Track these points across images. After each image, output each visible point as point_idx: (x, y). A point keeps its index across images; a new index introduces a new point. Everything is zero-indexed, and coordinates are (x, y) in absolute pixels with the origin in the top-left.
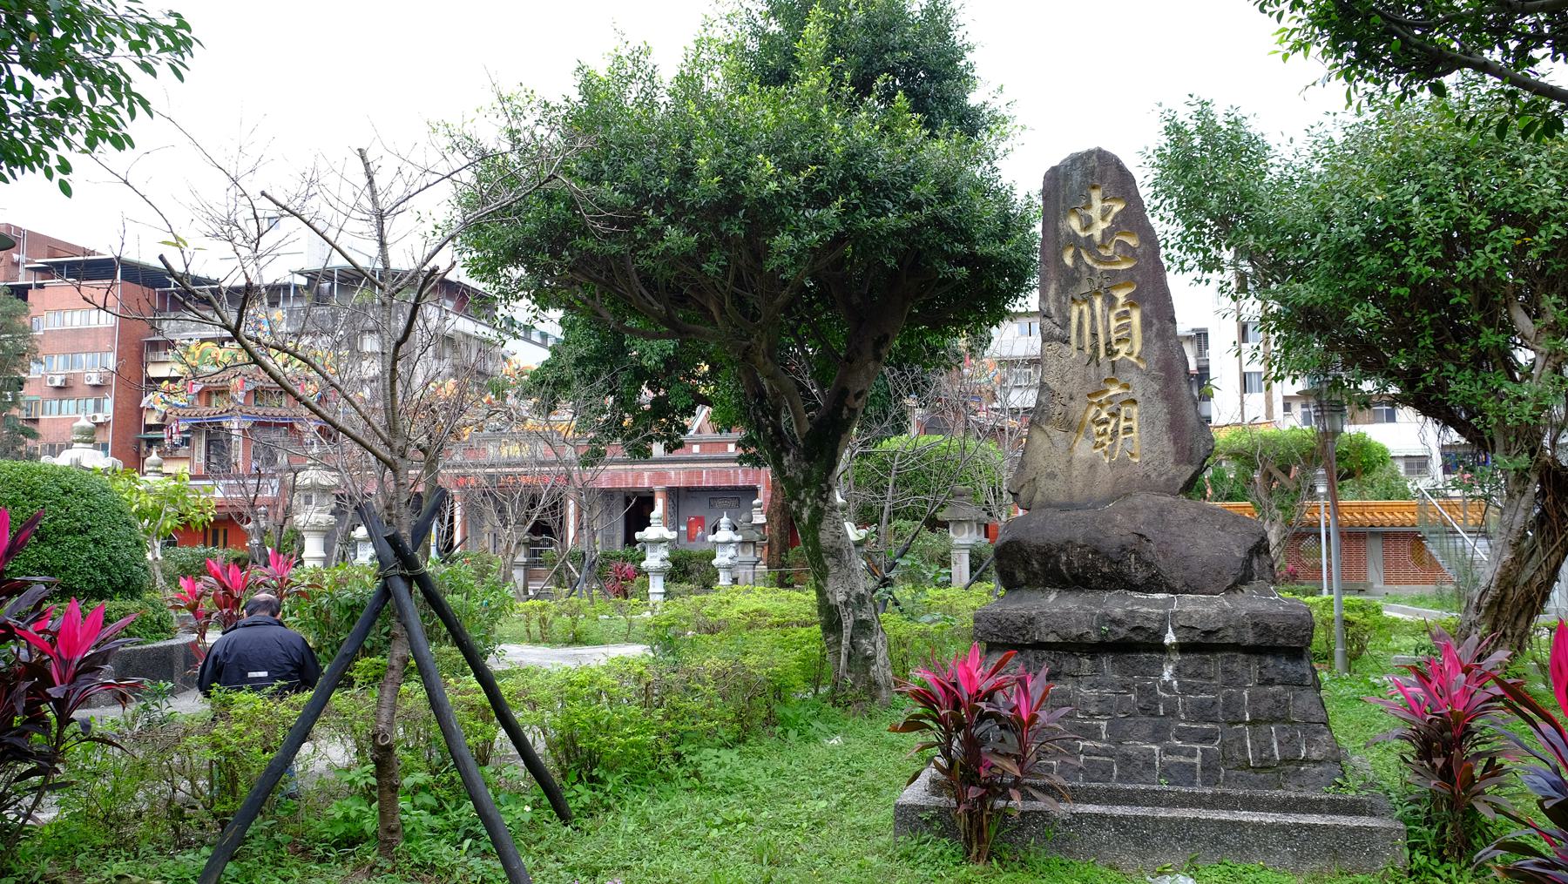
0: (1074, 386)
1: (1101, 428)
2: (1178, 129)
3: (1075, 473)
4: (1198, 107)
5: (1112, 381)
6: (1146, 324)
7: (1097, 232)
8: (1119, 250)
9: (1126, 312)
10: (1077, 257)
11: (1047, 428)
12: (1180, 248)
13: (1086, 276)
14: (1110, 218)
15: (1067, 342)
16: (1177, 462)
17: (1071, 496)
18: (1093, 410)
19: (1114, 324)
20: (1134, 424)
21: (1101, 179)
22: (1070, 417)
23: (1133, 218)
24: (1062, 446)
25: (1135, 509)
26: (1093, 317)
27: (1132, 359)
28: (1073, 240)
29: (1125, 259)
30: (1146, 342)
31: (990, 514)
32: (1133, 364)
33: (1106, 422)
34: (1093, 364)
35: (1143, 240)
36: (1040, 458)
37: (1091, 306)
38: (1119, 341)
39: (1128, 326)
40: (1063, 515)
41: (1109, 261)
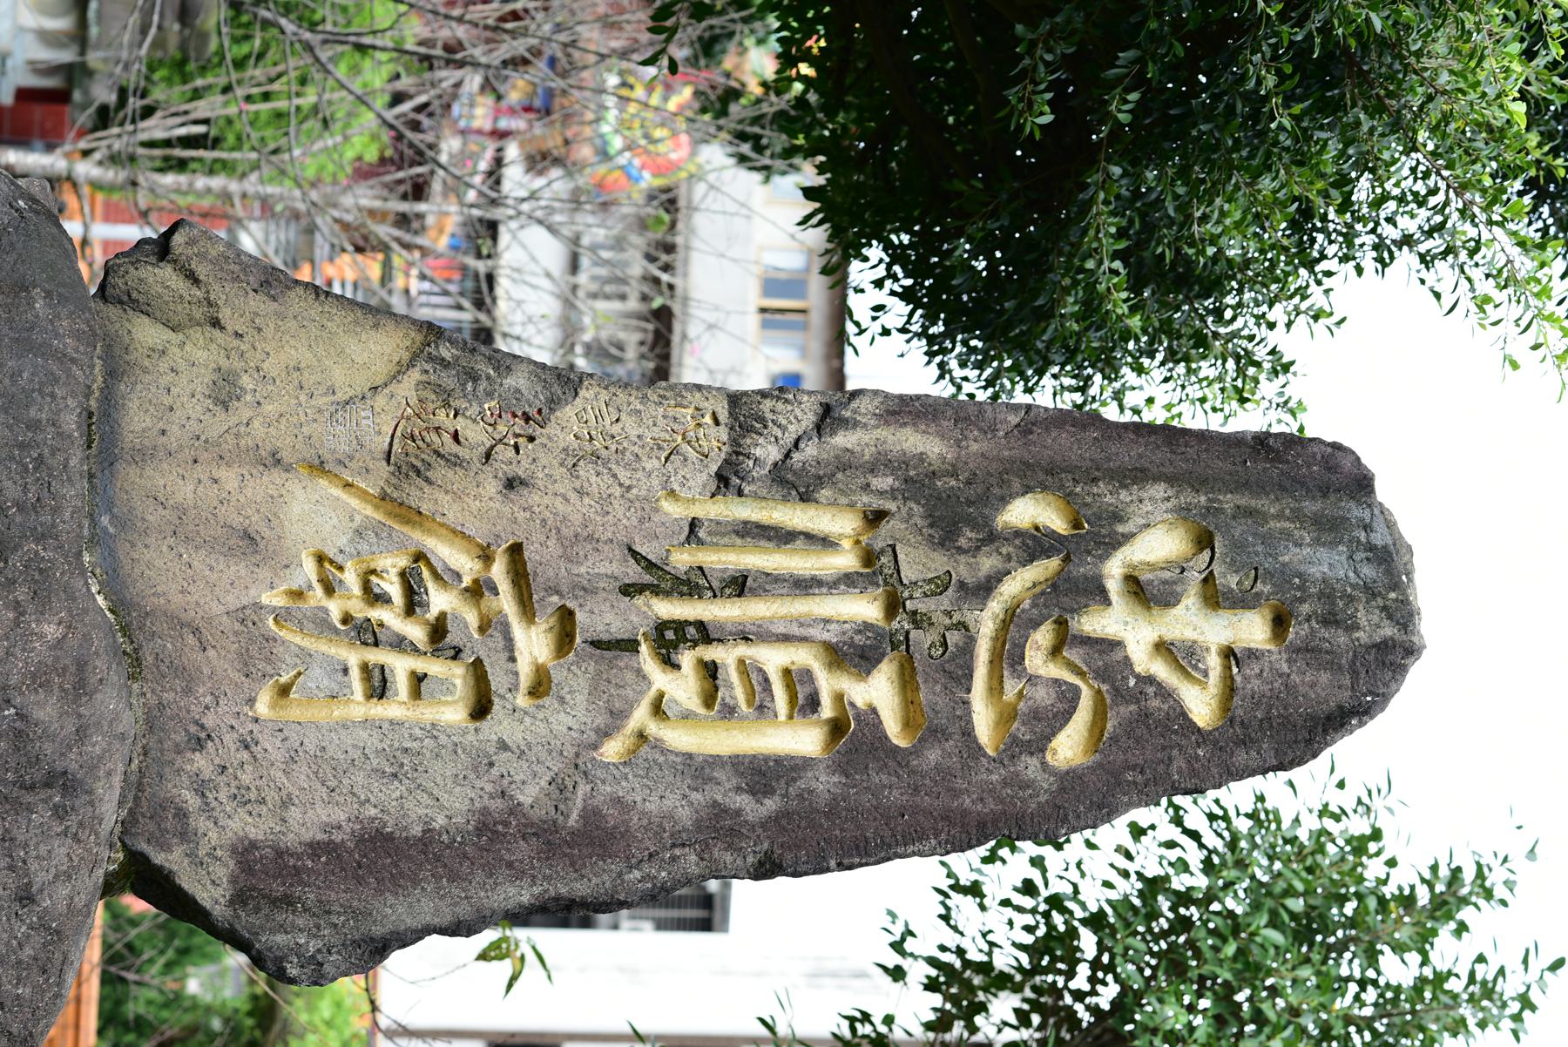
0: (559, 499)
1: (394, 590)
2: (1444, 907)
3: (229, 477)
4: (1510, 988)
5: (565, 636)
6: (763, 774)
7: (1114, 620)
8: (1043, 696)
9: (813, 703)
10: (1035, 544)
11: (407, 387)
12: (1028, 888)
13: (962, 570)
14: (1161, 670)
15: (726, 481)
16: (245, 852)
17: (143, 456)
18: (466, 565)
19: (773, 659)
20: (395, 708)
21: (1308, 651)
22: (440, 472)
23: (1150, 754)
24: (336, 439)
25: (81, 689)
26: (804, 586)
27: (640, 716)
28: (1100, 532)
29: (1007, 716)
30: (699, 769)
31: (104, 118)
32: (618, 716)
33: (413, 603)
34: (634, 573)
35: (1070, 779)
36: (296, 352)
37: (847, 581)
38: (710, 671)
39: (762, 709)
40: (71, 422)
41: (1008, 655)
